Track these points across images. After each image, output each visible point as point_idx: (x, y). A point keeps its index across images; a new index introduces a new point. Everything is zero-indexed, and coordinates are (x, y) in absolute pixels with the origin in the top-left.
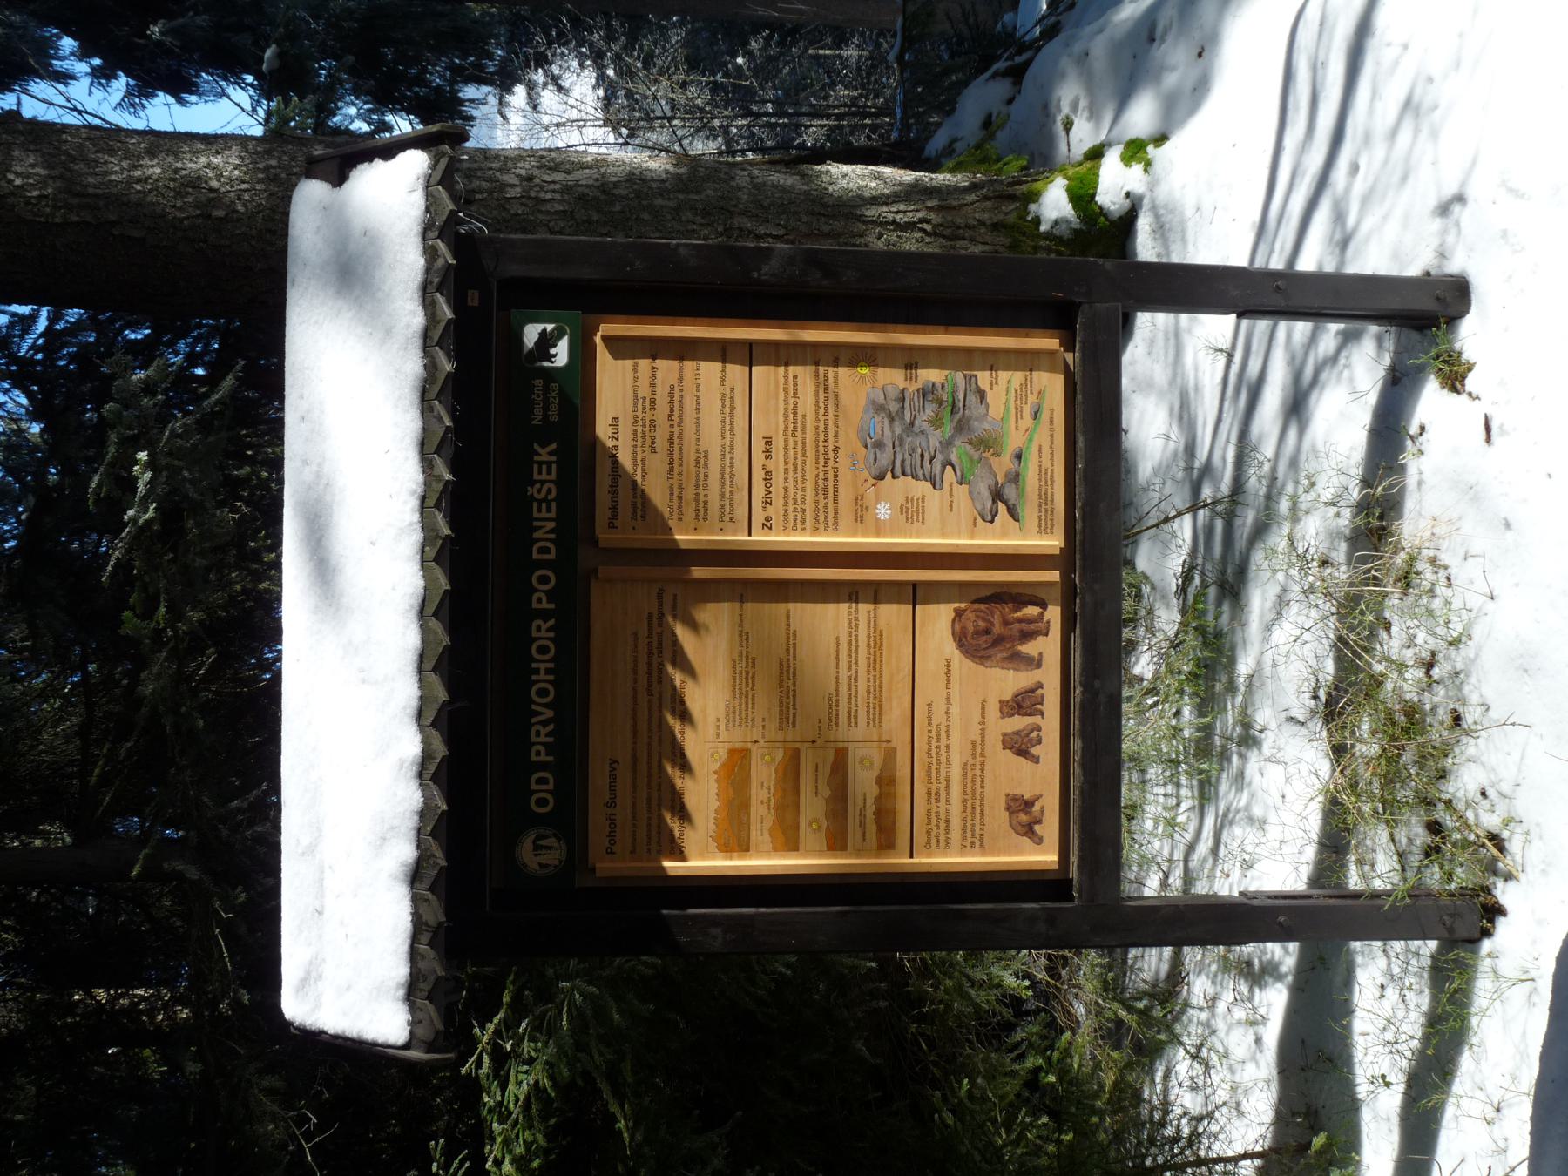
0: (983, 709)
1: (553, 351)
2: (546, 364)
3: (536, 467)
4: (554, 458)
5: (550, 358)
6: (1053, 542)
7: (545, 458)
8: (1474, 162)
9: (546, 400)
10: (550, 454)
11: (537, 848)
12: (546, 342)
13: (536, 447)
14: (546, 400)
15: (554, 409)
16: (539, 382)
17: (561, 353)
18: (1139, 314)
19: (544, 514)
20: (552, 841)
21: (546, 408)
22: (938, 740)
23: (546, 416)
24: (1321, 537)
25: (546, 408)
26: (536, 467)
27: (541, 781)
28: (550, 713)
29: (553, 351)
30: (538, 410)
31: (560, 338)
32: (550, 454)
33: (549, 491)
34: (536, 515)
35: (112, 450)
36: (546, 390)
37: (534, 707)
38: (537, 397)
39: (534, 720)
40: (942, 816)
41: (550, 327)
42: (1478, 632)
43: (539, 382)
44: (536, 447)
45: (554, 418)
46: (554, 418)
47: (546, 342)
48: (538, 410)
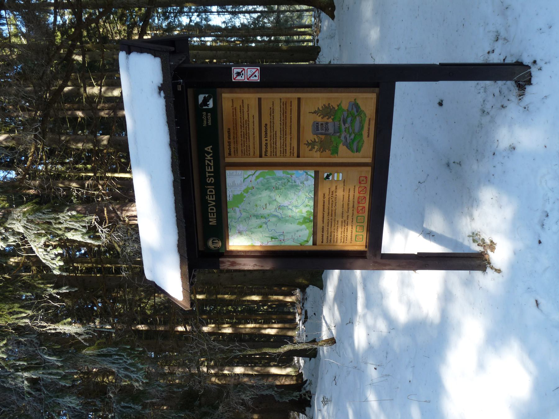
2: (206, 107)
5: (207, 105)
6: (369, 160)
7: (209, 158)
9: (207, 119)
10: (211, 157)
11: (213, 243)
12: (206, 101)
13: (206, 155)
14: (207, 119)
15: (210, 121)
17: (211, 104)
18: (397, 84)
19: (212, 217)
21: (207, 121)
22: (332, 207)
23: (207, 124)
25: (207, 121)
28: (214, 203)
30: (205, 122)
31: (210, 99)
32: (211, 157)
33: (212, 180)
34: (210, 217)
36: (207, 115)
38: (204, 117)
40: (334, 211)
41: (207, 95)
42: (507, 108)
43: (204, 113)
44: (206, 155)
45: (210, 124)
46: (210, 124)
47: (206, 101)
48: (205, 122)
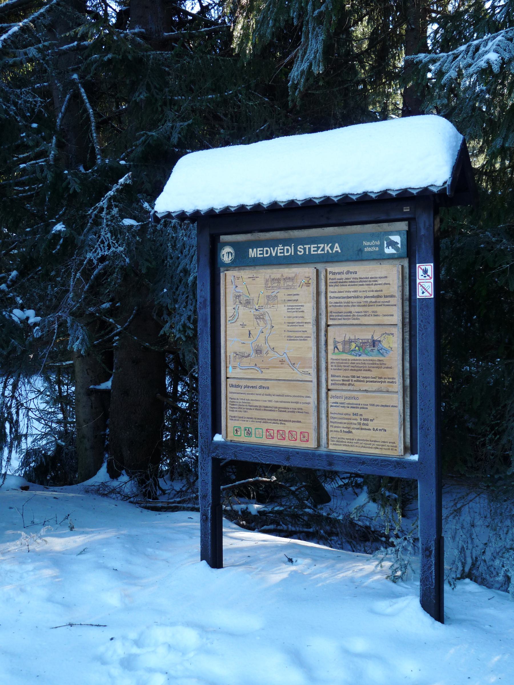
0: (296, 396)
1: (390, 247)
3: (262, 249)
4: (326, 252)
5: (388, 247)
8: (105, 626)
10: (328, 250)
11: (229, 253)
12: (392, 244)
13: (330, 245)
15: (369, 249)
16: (378, 243)
17: (390, 251)
19: (259, 252)
20: (230, 258)
21: (370, 246)
23: (366, 246)
24: (381, 556)
25: (370, 246)
26: (262, 249)
27: (288, 250)
29: (390, 247)
30: (368, 243)
32: (328, 250)
34: (258, 249)
35: (91, 110)
36: (376, 246)
37: (276, 248)
38: (373, 243)
39: (271, 248)
41: (399, 246)
44: (330, 245)
45: (293, 254)
46: (293, 254)
48: (368, 243)
